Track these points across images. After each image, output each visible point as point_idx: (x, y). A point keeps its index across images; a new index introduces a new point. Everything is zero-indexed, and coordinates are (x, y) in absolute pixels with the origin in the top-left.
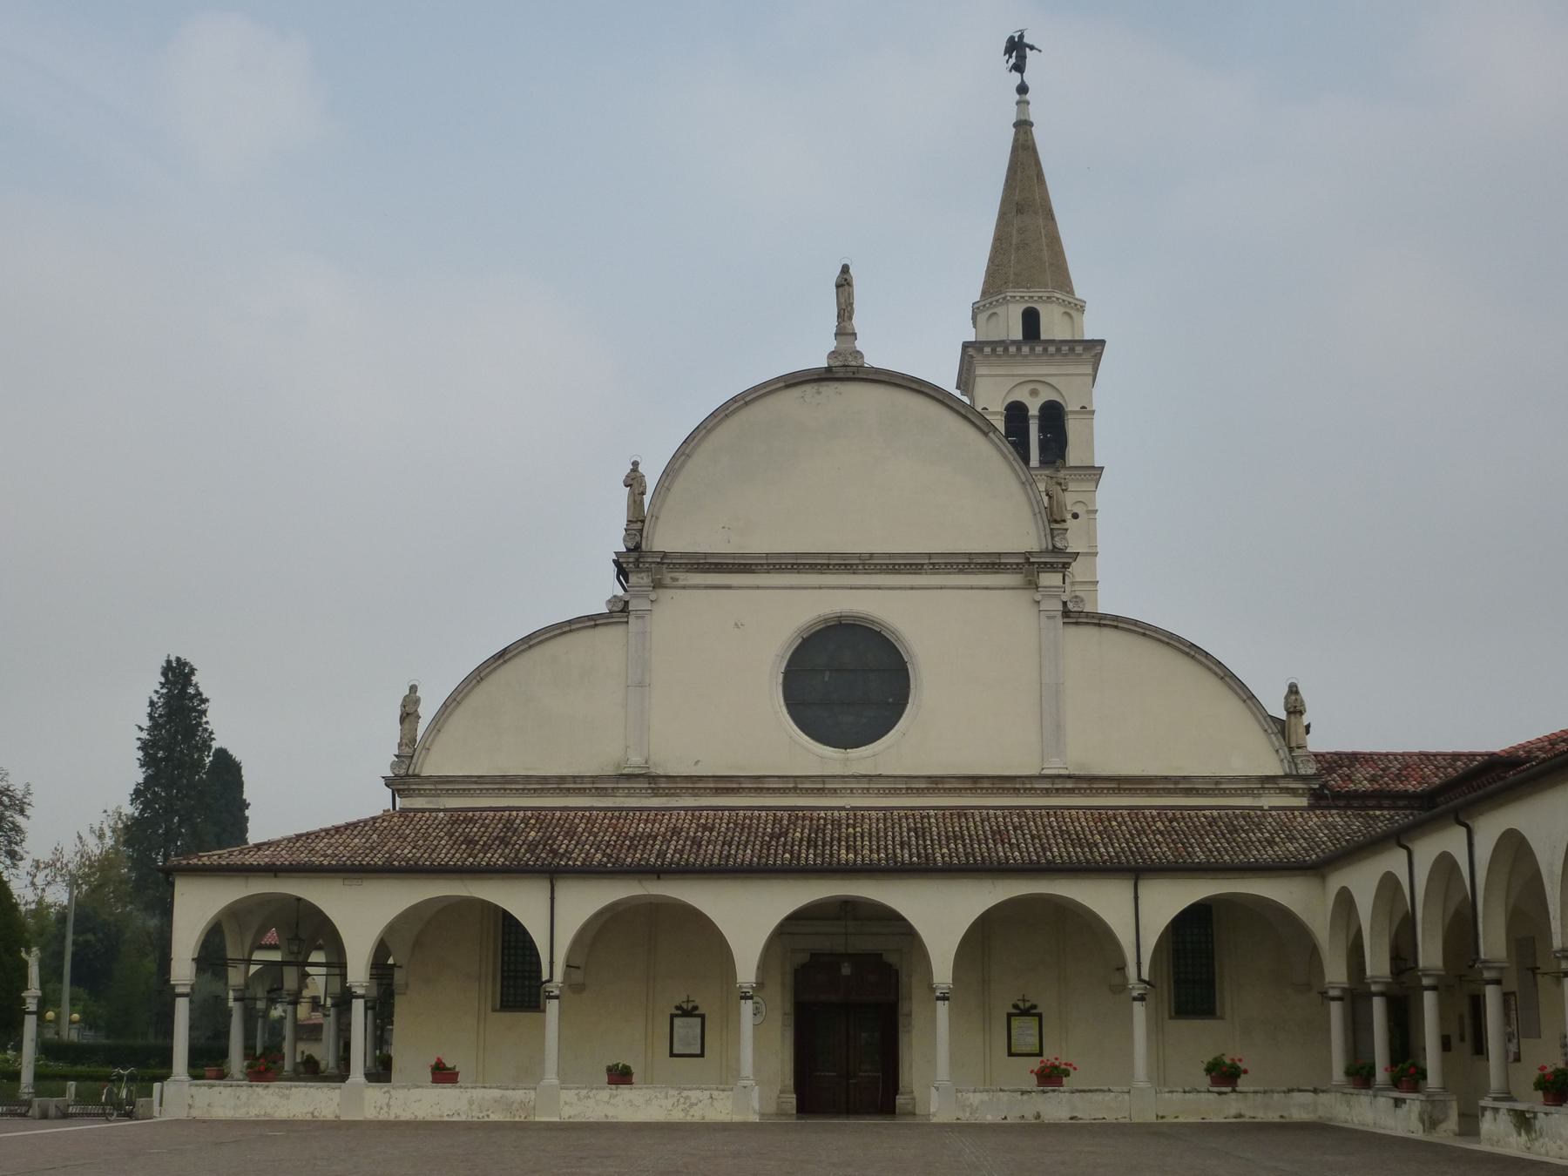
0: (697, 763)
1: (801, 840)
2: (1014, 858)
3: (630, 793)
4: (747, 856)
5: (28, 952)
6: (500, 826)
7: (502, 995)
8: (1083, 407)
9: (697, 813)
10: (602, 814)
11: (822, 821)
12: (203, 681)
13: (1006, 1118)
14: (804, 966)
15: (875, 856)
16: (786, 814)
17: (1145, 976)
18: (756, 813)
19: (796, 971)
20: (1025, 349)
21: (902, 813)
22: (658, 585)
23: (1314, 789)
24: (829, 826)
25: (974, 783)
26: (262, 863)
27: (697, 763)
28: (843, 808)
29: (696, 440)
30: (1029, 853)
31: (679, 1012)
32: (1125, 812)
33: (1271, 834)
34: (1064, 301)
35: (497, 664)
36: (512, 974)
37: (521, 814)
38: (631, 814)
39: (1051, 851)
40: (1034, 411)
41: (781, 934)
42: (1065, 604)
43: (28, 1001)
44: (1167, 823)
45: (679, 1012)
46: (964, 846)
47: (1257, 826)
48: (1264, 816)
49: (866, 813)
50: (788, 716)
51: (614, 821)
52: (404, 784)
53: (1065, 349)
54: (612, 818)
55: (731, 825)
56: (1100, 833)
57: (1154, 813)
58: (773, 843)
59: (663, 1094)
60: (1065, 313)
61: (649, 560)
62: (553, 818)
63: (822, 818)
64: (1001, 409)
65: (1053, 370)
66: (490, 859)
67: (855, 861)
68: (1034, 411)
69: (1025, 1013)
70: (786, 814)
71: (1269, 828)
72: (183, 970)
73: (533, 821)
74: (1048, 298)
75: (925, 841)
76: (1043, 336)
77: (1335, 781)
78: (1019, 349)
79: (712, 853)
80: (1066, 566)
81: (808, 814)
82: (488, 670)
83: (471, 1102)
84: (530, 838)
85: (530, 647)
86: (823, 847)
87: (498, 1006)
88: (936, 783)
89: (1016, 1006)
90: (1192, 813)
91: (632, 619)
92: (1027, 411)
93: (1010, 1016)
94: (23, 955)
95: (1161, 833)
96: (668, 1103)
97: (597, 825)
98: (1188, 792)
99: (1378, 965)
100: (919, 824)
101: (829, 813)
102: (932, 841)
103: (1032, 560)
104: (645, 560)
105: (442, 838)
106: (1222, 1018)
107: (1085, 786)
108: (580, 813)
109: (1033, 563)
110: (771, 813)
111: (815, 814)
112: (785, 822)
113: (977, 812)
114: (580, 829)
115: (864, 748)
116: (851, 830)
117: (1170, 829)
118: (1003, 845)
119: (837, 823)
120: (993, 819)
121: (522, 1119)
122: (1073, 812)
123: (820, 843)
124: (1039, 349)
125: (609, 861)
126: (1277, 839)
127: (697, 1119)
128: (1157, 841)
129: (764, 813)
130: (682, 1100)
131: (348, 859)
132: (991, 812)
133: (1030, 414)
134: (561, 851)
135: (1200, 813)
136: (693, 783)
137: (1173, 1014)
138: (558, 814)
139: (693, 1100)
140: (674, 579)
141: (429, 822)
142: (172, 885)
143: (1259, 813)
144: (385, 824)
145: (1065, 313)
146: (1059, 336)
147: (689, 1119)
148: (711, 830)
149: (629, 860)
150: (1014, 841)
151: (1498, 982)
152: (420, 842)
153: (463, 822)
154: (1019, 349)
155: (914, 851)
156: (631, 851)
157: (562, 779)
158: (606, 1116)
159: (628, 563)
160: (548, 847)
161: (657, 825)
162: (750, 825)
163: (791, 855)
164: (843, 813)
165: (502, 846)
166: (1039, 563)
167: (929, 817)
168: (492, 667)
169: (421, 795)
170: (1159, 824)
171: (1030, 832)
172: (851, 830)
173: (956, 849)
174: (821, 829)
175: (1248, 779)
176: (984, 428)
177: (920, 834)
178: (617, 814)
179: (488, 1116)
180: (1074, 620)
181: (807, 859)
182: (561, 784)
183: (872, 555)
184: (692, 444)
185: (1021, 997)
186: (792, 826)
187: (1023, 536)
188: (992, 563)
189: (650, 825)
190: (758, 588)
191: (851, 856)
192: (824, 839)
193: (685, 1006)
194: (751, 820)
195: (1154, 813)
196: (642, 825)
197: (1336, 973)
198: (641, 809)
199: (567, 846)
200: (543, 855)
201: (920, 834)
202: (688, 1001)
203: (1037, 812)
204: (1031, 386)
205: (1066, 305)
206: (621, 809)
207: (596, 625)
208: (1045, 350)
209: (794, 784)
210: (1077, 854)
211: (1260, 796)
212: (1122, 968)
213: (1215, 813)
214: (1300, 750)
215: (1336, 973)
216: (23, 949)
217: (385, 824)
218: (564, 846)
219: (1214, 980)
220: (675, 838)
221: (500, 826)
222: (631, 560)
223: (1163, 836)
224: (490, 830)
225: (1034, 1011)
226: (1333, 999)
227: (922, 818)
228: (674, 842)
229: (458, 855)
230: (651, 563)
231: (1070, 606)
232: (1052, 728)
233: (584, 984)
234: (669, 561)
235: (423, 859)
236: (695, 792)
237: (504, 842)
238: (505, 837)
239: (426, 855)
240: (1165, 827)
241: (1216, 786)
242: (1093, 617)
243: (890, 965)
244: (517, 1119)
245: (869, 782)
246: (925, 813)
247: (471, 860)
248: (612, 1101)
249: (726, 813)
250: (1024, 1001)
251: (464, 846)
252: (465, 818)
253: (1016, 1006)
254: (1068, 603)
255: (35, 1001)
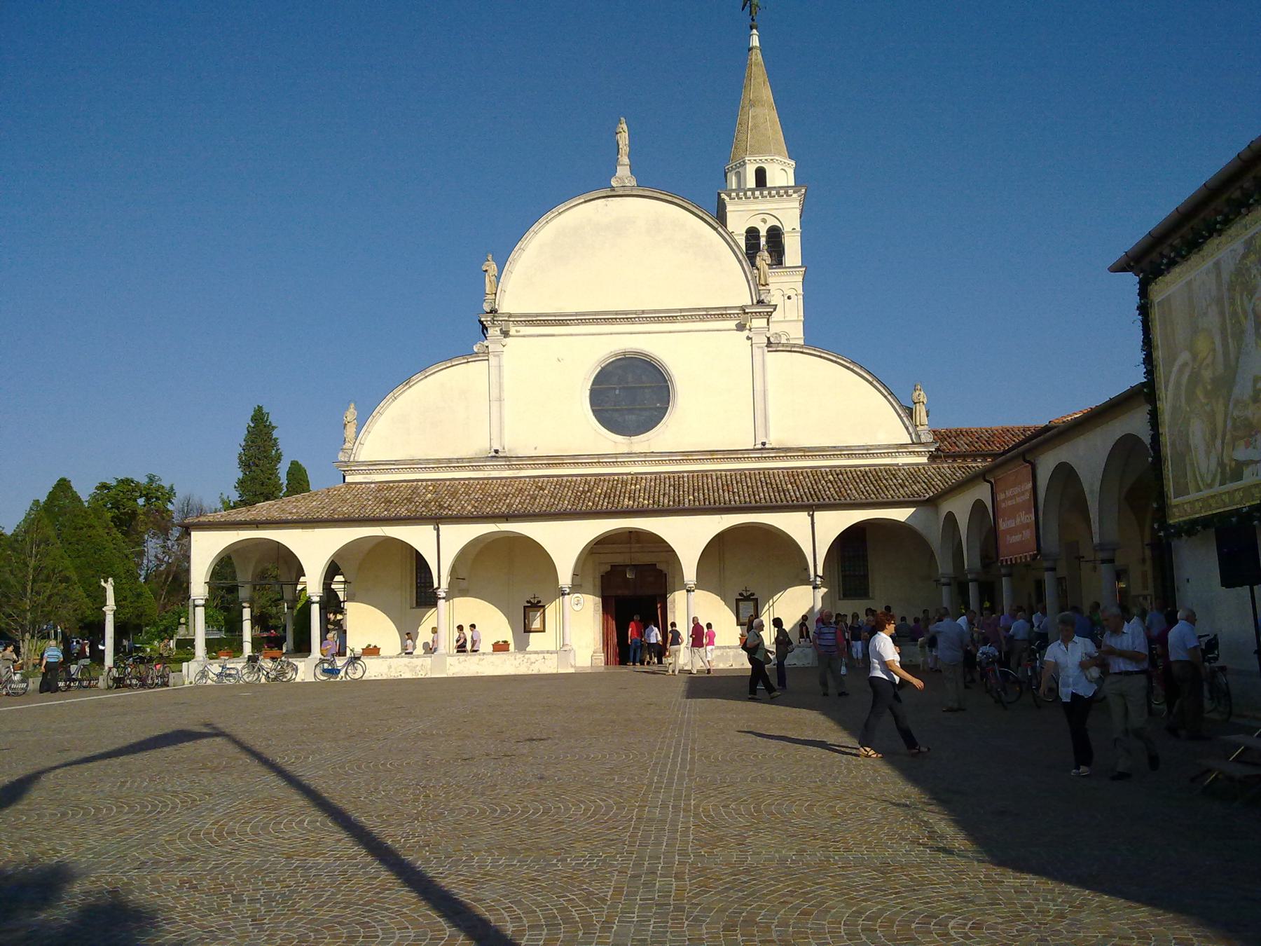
0: (536, 448)
1: (601, 494)
2: (735, 501)
3: (494, 468)
4: (566, 505)
5: (106, 582)
6: (409, 491)
7: (417, 598)
8: (794, 229)
9: (537, 480)
10: (476, 482)
11: (615, 482)
12: (273, 419)
13: (732, 665)
14: (607, 573)
15: (646, 502)
16: (593, 479)
17: (820, 572)
18: (574, 478)
19: (602, 576)
20: (757, 193)
21: (667, 475)
22: (506, 334)
23: (932, 452)
24: (620, 485)
25: (712, 454)
26: (248, 519)
27: (536, 448)
28: (630, 474)
29: (528, 239)
30: (744, 498)
31: (529, 605)
32: (809, 470)
33: (903, 480)
34: (781, 161)
35: (405, 388)
36: (422, 585)
37: (424, 483)
38: (495, 481)
39: (759, 495)
40: (763, 232)
41: (592, 553)
42: (769, 339)
43: (107, 612)
44: (835, 476)
45: (529, 605)
46: (704, 494)
47: (894, 475)
48: (899, 470)
49: (644, 476)
50: (594, 418)
51: (483, 486)
52: (348, 466)
53: (782, 192)
54: (482, 485)
55: (558, 486)
56: (791, 483)
57: (828, 470)
58: (583, 496)
59: (513, 657)
60: (782, 169)
61: (501, 319)
62: (444, 486)
63: (616, 480)
64: (743, 232)
65: (775, 206)
66: (398, 512)
67: (633, 506)
68: (763, 232)
69: (747, 599)
70: (593, 479)
71: (902, 476)
72: (199, 588)
73: (431, 488)
74: (771, 160)
75: (679, 492)
76: (768, 185)
77: (946, 446)
78: (753, 194)
79: (541, 504)
80: (769, 314)
81: (607, 478)
82: (400, 392)
83: (390, 667)
84: (427, 498)
85: (426, 377)
86: (614, 498)
87: (414, 606)
88: (687, 456)
89: (741, 594)
90: (853, 469)
91: (491, 357)
92: (759, 232)
93: (737, 600)
94: (103, 583)
95: (831, 482)
96: (516, 663)
97: (472, 489)
98: (849, 456)
99: (971, 560)
100: (676, 481)
101: (621, 477)
102: (684, 491)
103: (747, 311)
104: (498, 319)
105: (370, 500)
106: (872, 599)
107: (783, 455)
108: (462, 482)
109: (747, 313)
110: (584, 478)
111: (612, 478)
112: (592, 483)
113: (714, 473)
114: (460, 492)
115: (642, 436)
116: (633, 487)
117: (837, 479)
118: (728, 493)
119: (624, 483)
120: (724, 478)
121: (423, 677)
122: (776, 471)
123: (612, 495)
124: (766, 193)
125: (475, 511)
126: (907, 484)
127: (535, 672)
128: (828, 487)
129: (579, 478)
130: (525, 660)
131: (306, 514)
132: (723, 473)
133: (761, 234)
134: (446, 505)
135: (857, 469)
136: (534, 461)
137: (842, 596)
138: (448, 483)
139: (533, 660)
140: (517, 331)
141: (364, 491)
142: (190, 534)
143: (895, 467)
144: (335, 492)
145: (782, 169)
146: (777, 185)
147: (530, 672)
148: (544, 490)
149: (488, 509)
150: (736, 490)
151: (1053, 569)
152: (355, 503)
153: (386, 489)
154: (753, 194)
155: (672, 498)
156: (491, 504)
157: (450, 460)
158: (477, 672)
159: (487, 321)
160: (437, 503)
161: (510, 488)
162: (570, 486)
163: (593, 504)
164: (630, 477)
165: (408, 504)
166: (752, 313)
167: (683, 477)
168: (401, 391)
169: (360, 474)
170: (830, 477)
171: (747, 484)
172: (633, 487)
173: (699, 497)
174: (617, 486)
175: (888, 446)
176: (729, 240)
177: (676, 488)
178: (486, 482)
179: (401, 675)
180: (774, 349)
181: (602, 505)
182: (449, 463)
183: (643, 312)
184: (526, 242)
185: (744, 589)
186: (596, 486)
187: (743, 297)
188: (721, 314)
189: (505, 488)
190: (572, 335)
191: (631, 502)
192: (615, 493)
193: (532, 600)
194: (571, 483)
195: (828, 470)
196: (501, 488)
197: (944, 567)
198: (501, 478)
199: (450, 502)
200: (433, 508)
201: (676, 488)
202: (534, 598)
203: (752, 472)
204: (763, 216)
205: (782, 164)
206: (488, 479)
207: (468, 362)
208: (770, 193)
209: (599, 459)
210: (779, 499)
211: (896, 457)
212: (806, 569)
213: (867, 469)
214: (922, 427)
215: (944, 567)
216: (102, 580)
217: (335, 492)
218: (448, 502)
219: (868, 575)
220: (520, 495)
221: (409, 491)
222: (489, 319)
223: (832, 484)
224: (402, 494)
225: (540, 604)
226: (944, 585)
227: (679, 478)
228: (519, 498)
229: (378, 510)
230: (501, 321)
231: (772, 340)
232: (759, 414)
233: (581, 585)
234: (513, 319)
235: (354, 513)
236: (535, 466)
237: (410, 500)
238: (411, 498)
239: (357, 511)
240: (834, 478)
241: (867, 451)
242: (787, 346)
243: (661, 571)
244: (420, 676)
245: (646, 456)
246: (681, 475)
247: (386, 513)
248: (481, 662)
249: (555, 479)
250: (746, 591)
251: (383, 505)
252: (387, 488)
253: (741, 594)
254: (771, 338)
255: (112, 612)
